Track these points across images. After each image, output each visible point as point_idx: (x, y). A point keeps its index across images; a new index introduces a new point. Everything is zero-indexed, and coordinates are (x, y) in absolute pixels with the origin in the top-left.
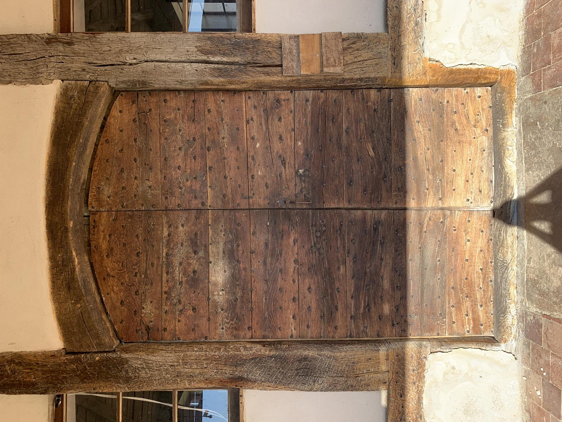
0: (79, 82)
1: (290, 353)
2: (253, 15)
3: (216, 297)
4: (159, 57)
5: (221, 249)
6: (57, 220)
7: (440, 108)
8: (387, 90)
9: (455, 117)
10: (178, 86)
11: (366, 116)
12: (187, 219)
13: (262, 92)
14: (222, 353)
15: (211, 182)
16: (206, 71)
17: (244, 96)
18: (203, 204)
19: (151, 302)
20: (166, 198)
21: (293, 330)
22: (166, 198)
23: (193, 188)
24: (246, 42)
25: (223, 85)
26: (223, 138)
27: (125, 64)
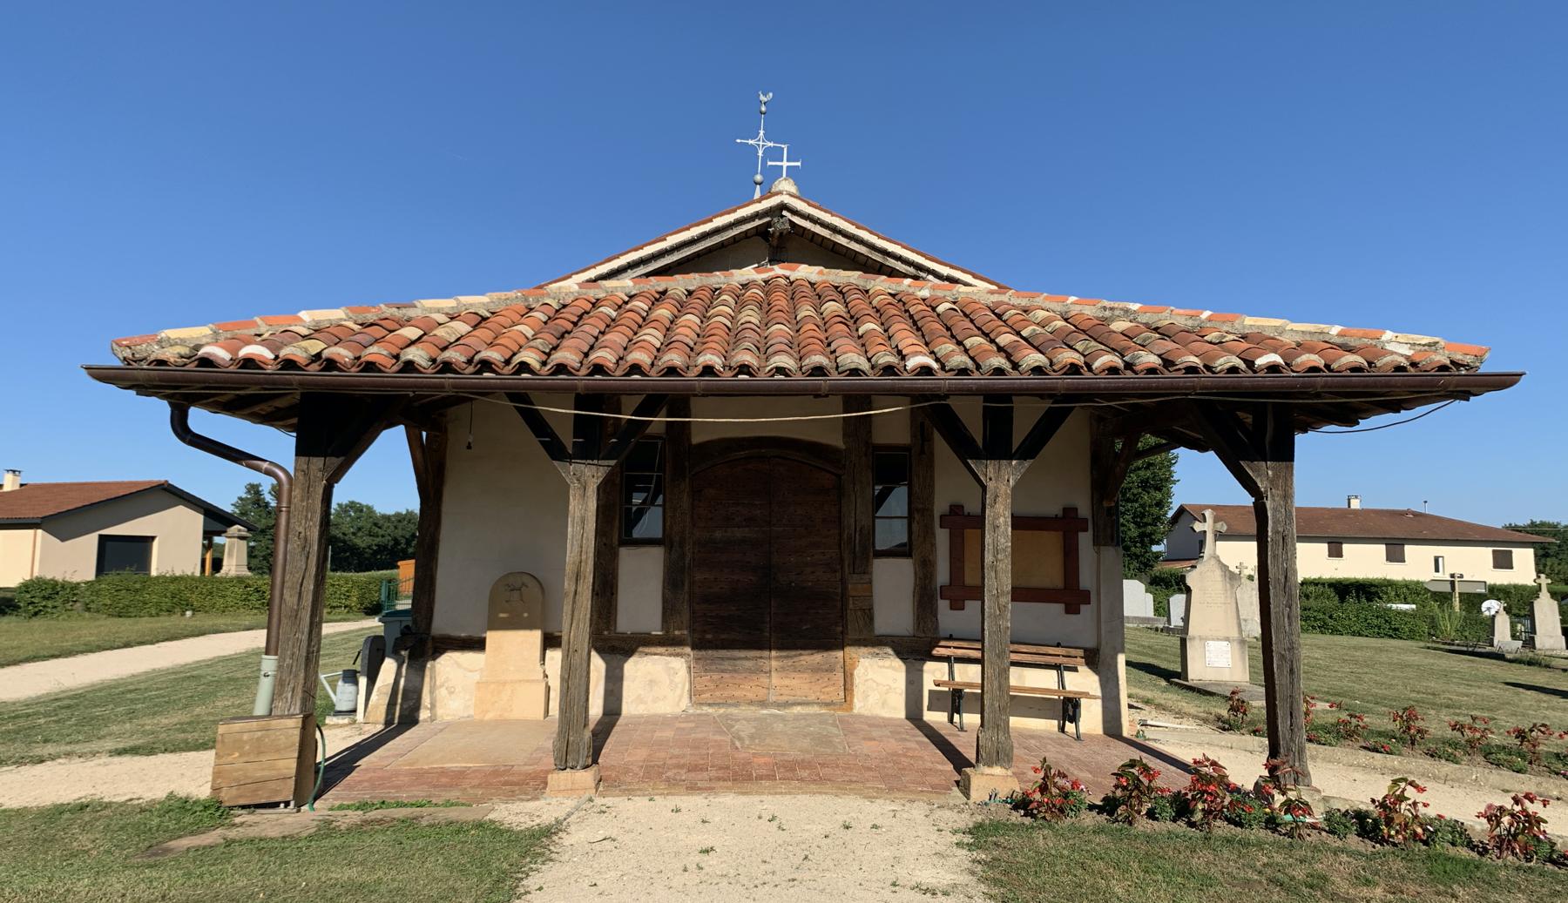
7: (831, 670)
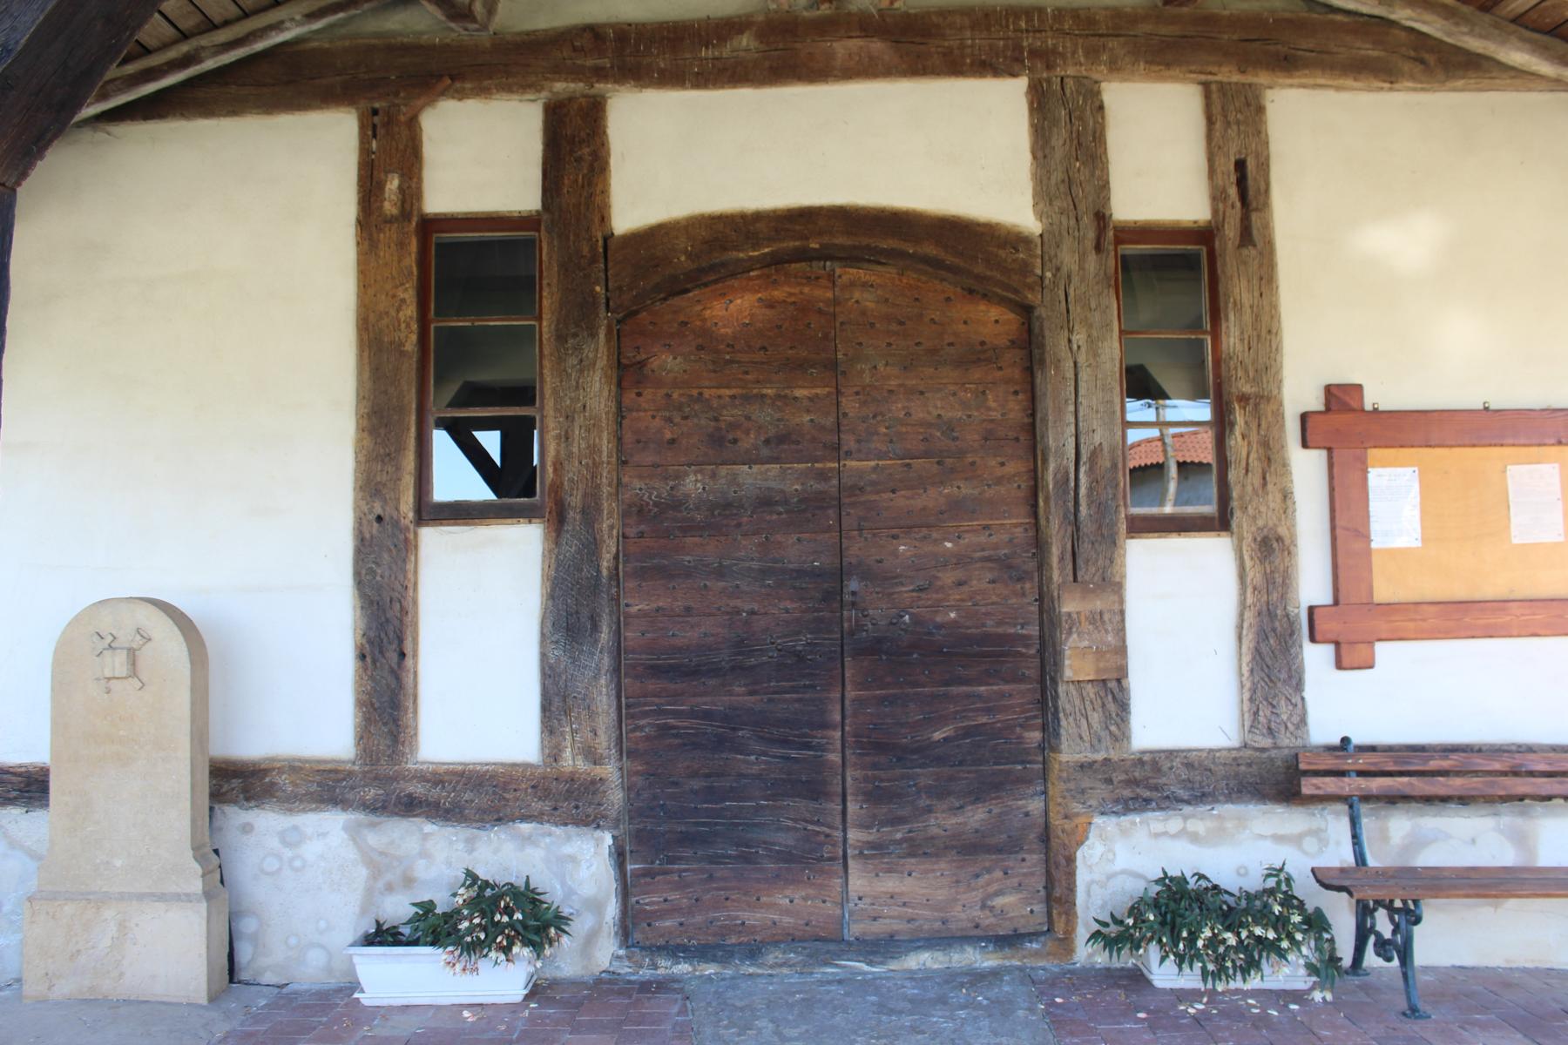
3: (692, 478)
5: (773, 484)
9: (998, 874)
10: (1039, 416)
12: (822, 428)
14: (606, 490)
15: (884, 468)
18: (849, 454)
20: (857, 393)
22: (857, 393)
24: (1113, 524)
27: (1071, 331)
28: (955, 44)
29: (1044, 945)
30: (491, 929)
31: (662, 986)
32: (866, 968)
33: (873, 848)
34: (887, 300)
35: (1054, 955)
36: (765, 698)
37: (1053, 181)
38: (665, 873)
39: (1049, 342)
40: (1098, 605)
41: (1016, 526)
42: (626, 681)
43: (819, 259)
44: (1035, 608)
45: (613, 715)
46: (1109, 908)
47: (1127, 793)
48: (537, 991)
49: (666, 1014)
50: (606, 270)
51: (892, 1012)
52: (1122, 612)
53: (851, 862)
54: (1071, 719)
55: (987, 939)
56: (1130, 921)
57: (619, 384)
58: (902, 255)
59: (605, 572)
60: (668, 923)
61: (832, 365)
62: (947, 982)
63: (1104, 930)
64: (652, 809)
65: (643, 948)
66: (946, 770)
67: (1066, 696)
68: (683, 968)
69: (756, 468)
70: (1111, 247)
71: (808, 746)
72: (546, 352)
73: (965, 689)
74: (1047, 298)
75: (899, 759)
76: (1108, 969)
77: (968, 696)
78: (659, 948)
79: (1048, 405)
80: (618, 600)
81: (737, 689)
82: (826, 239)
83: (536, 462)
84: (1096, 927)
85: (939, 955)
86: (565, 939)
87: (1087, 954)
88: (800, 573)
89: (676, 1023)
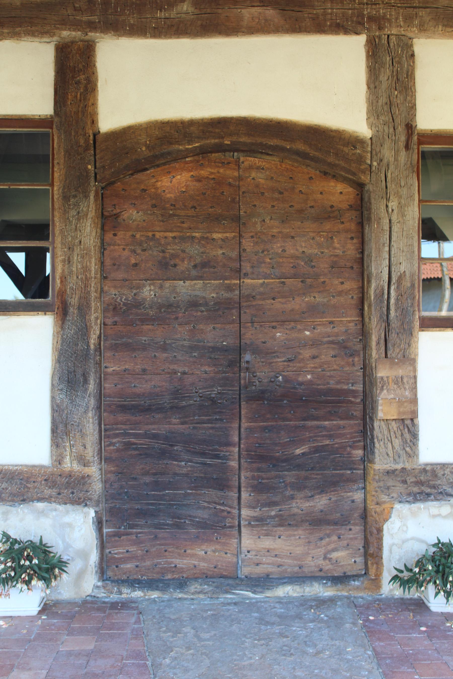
0: (369, 155)
1: (92, 365)
2: (438, 329)
4: (394, 235)
5: (197, 293)
6: (232, 128)
8: (362, 467)
9: (335, 538)
10: (366, 253)
11: (336, 446)
12: (231, 258)
13: (361, 338)
14: (93, 295)
15: (268, 284)
16: (380, 281)
17: (357, 319)
18: (246, 275)
19: (144, 221)
20: (252, 237)
21: (112, 369)
22: (252, 237)
23: (263, 265)
24: (411, 322)
25: (367, 298)
26: (315, 297)
27: (388, 200)
28: (320, 12)
29: (363, 583)
30: (18, 570)
31: (124, 605)
32: (251, 595)
33: (257, 520)
34: (272, 178)
35: (369, 589)
36: (191, 426)
37: (380, 104)
38: (127, 534)
39: (374, 207)
40: (400, 372)
41: (350, 322)
42: (105, 415)
43: (230, 151)
44: (360, 374)
45: (97, 436)
46: (403, 561)
47: (416, 489)
48: (47, 608)
49: (127, 623)
50: (95, 155)
51: (267, 623)
52: (415, 377)
53: (243, 529)
54: (382, 443)
55: (327, 578)
56: (417, 570)
57: (103, 228)
58: (283, 149)
59: (92, 347)
60: (129, 566)
61: (237, 219)
62: (302, 605)
63: (400, 575)
64: (120, 494)
65: (113, 581)
66: (303, 473)
67: (379, 428)
68: (138, 594)
69: (188, 283)
70: (416, 147)
71: (217, 457)
72: (56, 206)
73: (316, 423)
74: (373, 179)
75: (274, 466)
76: (402, 599)
77: (318, 427)
78: (123, 581)
79: (371, 246)
80: (100, 364)
81: (174, 421)
82: (235, 139)
83: (48, 271)
84: (395, 573)
85: (297, 588)
86: (64, 576)
87: (389, 589)
88: (214, 349)
89: (133, 630)
